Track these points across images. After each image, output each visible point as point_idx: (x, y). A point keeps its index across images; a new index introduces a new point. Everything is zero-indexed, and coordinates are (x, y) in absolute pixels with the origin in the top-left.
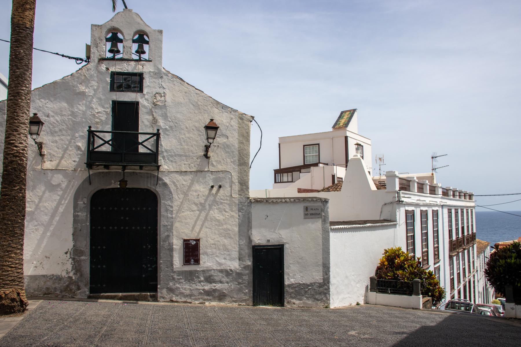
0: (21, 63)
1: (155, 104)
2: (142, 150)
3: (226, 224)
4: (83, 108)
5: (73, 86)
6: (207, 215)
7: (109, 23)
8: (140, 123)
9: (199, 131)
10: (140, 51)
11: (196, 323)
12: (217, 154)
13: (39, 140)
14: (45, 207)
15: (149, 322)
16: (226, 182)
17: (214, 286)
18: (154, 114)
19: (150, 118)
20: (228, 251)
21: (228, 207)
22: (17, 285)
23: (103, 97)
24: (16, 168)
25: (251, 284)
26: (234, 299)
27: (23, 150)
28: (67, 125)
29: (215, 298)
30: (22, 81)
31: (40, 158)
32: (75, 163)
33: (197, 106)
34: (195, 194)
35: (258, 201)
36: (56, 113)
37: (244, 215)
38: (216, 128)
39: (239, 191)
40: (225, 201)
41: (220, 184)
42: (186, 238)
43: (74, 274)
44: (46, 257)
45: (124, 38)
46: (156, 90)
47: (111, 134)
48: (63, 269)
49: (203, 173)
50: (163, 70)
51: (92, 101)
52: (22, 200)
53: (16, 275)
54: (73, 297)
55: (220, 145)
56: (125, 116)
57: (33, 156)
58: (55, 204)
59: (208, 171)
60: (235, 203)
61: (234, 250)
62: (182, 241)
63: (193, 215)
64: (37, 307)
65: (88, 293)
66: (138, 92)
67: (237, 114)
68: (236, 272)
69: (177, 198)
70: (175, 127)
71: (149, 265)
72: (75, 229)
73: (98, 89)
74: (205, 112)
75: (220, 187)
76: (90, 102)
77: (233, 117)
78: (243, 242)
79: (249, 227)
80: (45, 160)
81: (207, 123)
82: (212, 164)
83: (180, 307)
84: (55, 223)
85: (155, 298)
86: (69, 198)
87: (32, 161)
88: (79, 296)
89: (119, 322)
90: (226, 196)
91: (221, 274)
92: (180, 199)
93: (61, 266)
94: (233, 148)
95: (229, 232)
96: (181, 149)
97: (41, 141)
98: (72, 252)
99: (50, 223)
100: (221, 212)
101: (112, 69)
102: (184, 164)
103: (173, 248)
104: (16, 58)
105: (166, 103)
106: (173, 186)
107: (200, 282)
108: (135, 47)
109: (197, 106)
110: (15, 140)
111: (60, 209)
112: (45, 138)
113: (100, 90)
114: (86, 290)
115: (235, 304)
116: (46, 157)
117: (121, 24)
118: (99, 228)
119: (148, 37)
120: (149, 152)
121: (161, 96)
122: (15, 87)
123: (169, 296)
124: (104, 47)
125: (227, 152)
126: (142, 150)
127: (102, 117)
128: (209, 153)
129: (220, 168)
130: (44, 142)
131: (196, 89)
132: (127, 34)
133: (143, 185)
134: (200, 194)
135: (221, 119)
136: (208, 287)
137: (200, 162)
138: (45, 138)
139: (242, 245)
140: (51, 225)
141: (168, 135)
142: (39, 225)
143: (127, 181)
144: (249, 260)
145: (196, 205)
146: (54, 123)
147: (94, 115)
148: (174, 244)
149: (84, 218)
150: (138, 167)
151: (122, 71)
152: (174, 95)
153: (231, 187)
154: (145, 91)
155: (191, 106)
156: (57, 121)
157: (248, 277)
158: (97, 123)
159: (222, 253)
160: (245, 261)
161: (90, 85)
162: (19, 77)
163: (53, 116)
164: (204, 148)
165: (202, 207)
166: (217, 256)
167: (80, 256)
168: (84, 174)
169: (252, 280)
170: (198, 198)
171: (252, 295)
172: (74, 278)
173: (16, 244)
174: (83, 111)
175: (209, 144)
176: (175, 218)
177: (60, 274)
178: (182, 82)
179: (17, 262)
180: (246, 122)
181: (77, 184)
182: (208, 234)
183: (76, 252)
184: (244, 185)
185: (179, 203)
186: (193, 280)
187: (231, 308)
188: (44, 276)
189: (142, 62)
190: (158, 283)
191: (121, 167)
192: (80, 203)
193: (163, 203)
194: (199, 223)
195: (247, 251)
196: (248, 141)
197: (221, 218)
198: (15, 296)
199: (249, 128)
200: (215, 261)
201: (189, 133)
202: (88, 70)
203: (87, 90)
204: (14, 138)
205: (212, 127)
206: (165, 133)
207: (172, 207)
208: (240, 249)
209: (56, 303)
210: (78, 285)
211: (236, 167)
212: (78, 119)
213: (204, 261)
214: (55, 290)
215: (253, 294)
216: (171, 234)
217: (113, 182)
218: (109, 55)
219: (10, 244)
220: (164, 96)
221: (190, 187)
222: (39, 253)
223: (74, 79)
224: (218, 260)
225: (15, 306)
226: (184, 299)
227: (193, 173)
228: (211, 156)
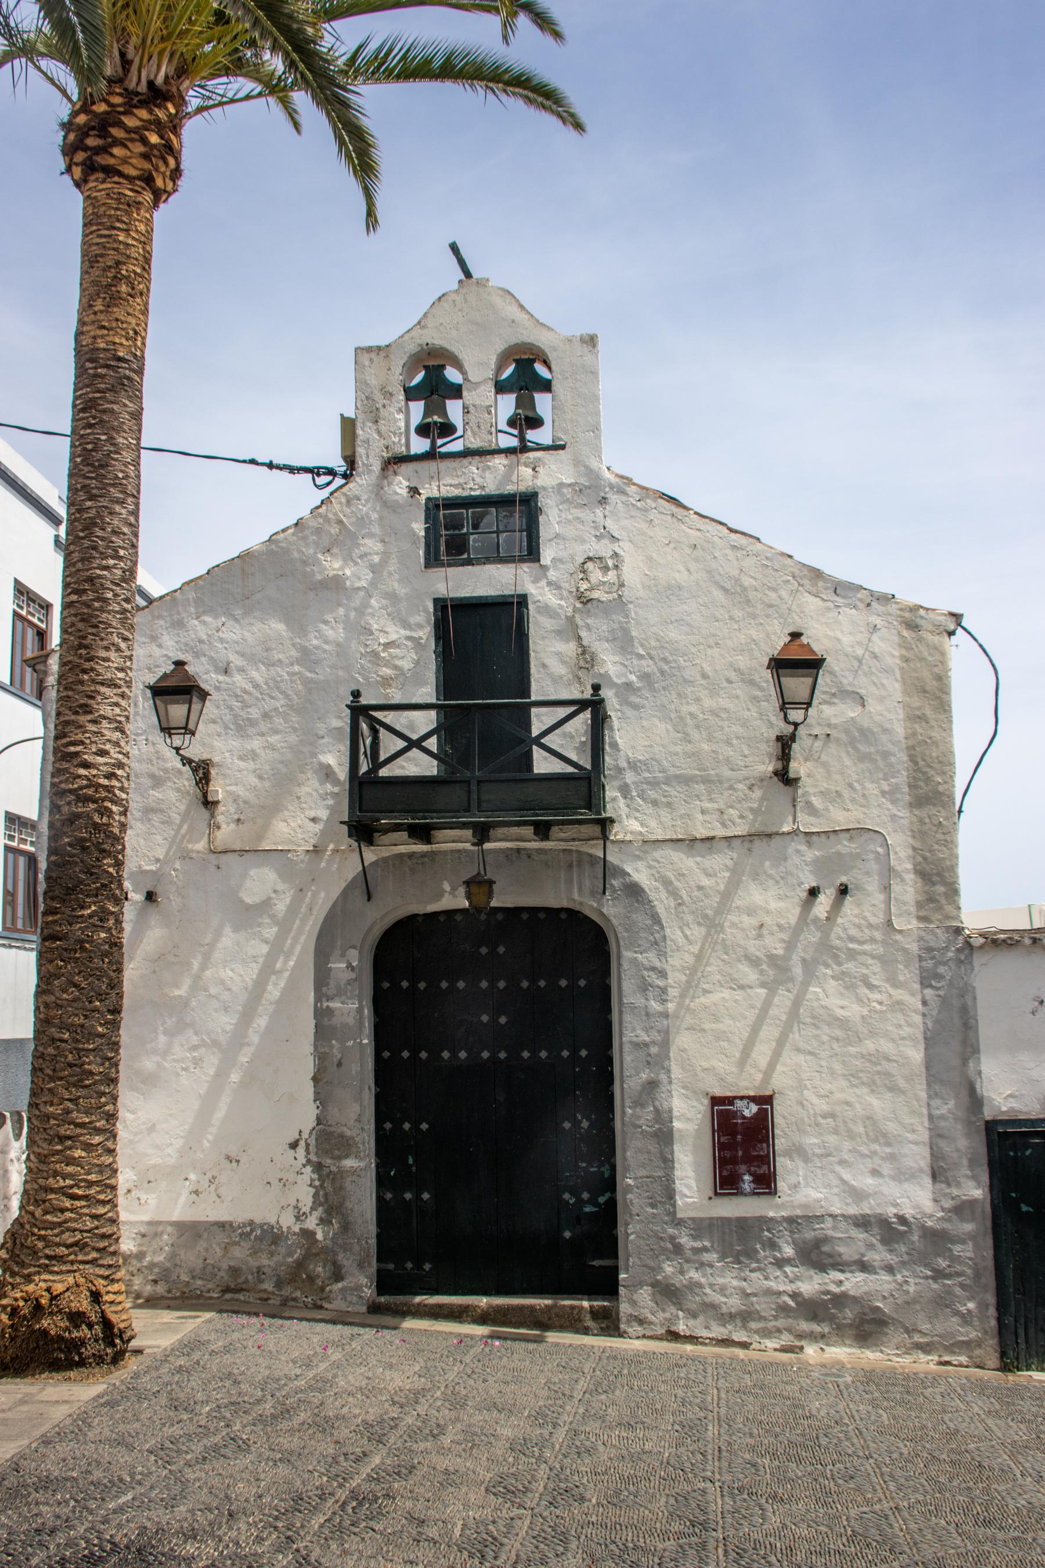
0: (100, 477)
1: (584, 600)
2: (543, 764)
3: (872, 1034)
4: (334, 632)
5: (304, 563)
6: (797, 1003)
7: (413, 333)
8: (533, 670)
9: (752, 683)
10: (526, 421)
11: (753, 1449)
12: (825, 765)
13: (195, 751)
14: (222, 982)
15: (560, 1435)
16: (868, 873)
17: (832, 1281)
18: (583, 634)
19: (570, 648)
20: (888, 1144)
21: (877, 967)
22: (93, 1262)
23: (402, 591)
24: (84, 840)
25: (989, 1279)
26: (918, 1338)
27: (110, 776)
28: (287, 696)
29: (840, 1332)
30: (102, 539)
31: (205, 813)
32: (318, 827)
33: (736, 592)
34: (747, 921)
35: (999, 943)
36: (252, 659)
37: (944, 1001)
38: (812, 665)
39: (919, 905)
40: (867, 947)
41: (844, 879)
42: (719, 1092)
43: (322, 1221)
44: (229, 1159)
45: (466, 379)
46: (587, 546)
47: (433, 714)
48: (284, 1203)
49: (776, 841)
50: (607, 475)
51: (366, 605)
52: (106, 954)
53: (90, 1224)
54: (317, 1309)
55: (834, 733)
56: (479, 645)
57: (183, 807)
58: (253, 971)
59: (795, 832)
60: (905, 951)
61: (910, 1136)
62: (706, 1102)
63: (741, 1003)
64: (180, 1341)
65: (369, 1292)
66: (522, 560)
67: (893, 608)
68: (923, 1228)
69: (683, 938)
70: (661, 677)
71: (585, 1196)
72: (321, 1058)
73: (384, 562)
74: (771, 611)
75: (844, 891)
76: (361, 611)
77: (875, 620)
78: (946, 1107)
79: (970, 1048)
80: (220, 818)
81: (776, 653)
82: (809, 804)
83: (702, 1361)
84: (254, 1037)
85: (609, 1323)
86: (299, 948)
87: (180, 826)
88: (338, 1304)
89: (441, 1429)
90: (870, 926)
91: (860, 1235)
92: (691, 942)
93: (277, 1196)
94: (884, 738)
95: (886, 1066)
96: (688, 755)
97: (205, 757)
98: (313, 1142)
99: (239, 1037)
100: (851, 987)
101: (430, 490)
102: (703, 812)
103: (671, 1131)
104: (86, 462)
105: (626, 592)
106: (664, 895)
107: (780, 1263)
108: (507, 405)
109: (736, 592)
110: (82, 743)
111: (270, 988)
112: (218, 744)
113: (393, 566)
114: (364, 1280)
115: (923, 1358)
116: (221, 808)
117: (454, 333)
118: (406, 1054)
119: (550, 368)
120: (570, 769)
121: (606, 569)
122: (82, 560)
123: (661, 1315)
124: (401, 416)
125: (863, 758)
126: (543, 764)
127: (404, 661)
128: (793, 765)
129: (840, 818)
130: (216, 759)
131: (731, 530)
132: (477, 365)
133: (552, 896)
134: (768, 920)
135: (829, 632)
136: (811, 1284)
137: (763, 799)
138: (218, 744)
139: (942, 1117)
140: (242, 1045)
141: (636, 707)
142: (203, 1044)
143: (491, 883)
144: (974, 1177)
145: (754, 962)
146: (245, 692)
147: (375, 654)
148: (675, 1113)
149: (351, 1021)
150: (529, 831)
151: (465, 494)
152: (650, 559)
153: (887, 889)
154: (547, 555)
155: (718, 594)
156: (256, 686)
157: (972, 1249)
158: (386, 682)
159: (863, 1149)
160: (958, 1185)
161: (357, 552)
162: (95, 524)
163: (241, 670)
164: (774, 748)
165: (776, 970)
166: (842, 1162)
167: (340, 1158)
168: (346, 863)
169: (990, 1263)
170: (760, 936)
171: (993, 1323)
172: (320, 1236)
173: (87, 1113)
174: (338, 645)
175: (791, 728)
176: (676, 1016)
177: (273, 1221)
178: (679, 511)
179: (93, 1177)
180: (929, 637)
181: (323, 898)
182: (804, 1076)
183: (327, 1142)
184: (938, 879)
185: (690, 959)
186: (751, 1254)
187: (907, 1378)
188: (222, 1225)
189: (532, 455)
190: (621, 1263)
191: (468, 833)
192: (338, 966)
193: (630, 962)
194: (769, 1033)
195: (962, 1143)
196: (943, 706)
197: (853, 1011)
198: (83, 1303)
199: (943, 662)
200: (836, 1182)
201: (713, 693)
202: (349, 502)
203: (348, 572)
204: (80, 737)
205: (797, 664)
206: (625, 702)
207: (662, 974)
208: (937, 1135)
209: (248, 1330)
210: (335, 1263)
211: (903, 813)
212: (323, 673)
213: (792, 1179)
214: (244, 1278)
215: (999, 1320)
216: (663, 1077)
217: (447, 887)
218: (420, 445)
219: (68, 1112)
220: (616, 567)
221: (727, 896)
222: (206, 1144)
223: (304, 538)
224: (846, 1176)
225: (83, 1342)
226: (718, 1331)
227: (736, 843)
228: (802, 773)
